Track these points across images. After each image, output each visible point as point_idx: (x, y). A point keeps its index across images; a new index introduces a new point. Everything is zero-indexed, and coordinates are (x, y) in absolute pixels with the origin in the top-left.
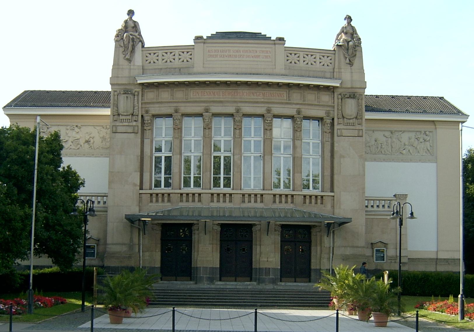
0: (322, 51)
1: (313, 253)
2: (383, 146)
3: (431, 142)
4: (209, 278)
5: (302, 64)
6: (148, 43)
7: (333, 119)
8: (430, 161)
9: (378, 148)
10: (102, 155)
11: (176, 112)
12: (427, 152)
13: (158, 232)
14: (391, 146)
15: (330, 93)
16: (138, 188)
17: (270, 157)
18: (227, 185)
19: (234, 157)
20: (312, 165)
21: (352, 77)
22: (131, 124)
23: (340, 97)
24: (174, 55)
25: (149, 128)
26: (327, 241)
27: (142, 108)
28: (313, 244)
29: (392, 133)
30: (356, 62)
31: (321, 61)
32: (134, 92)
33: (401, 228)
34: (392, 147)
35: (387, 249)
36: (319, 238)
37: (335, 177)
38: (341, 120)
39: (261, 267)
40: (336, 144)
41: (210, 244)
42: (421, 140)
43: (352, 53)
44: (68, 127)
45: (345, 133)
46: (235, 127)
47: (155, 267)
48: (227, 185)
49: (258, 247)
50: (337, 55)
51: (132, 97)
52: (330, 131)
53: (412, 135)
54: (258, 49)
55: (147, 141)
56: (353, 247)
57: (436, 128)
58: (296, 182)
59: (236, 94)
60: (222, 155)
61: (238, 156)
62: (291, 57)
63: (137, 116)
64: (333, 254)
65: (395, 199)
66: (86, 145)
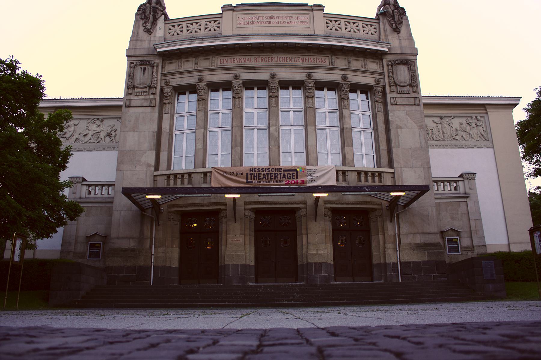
0: (364, 20)
1: (374, 244)
2: (434, 132)
6: (172, 14)
9: (428, 134)
12: (482, 137)
13: (176, 223)
14: (443, 131)
15: (378, 61)
16: (153, 169)
17: (313, 127)
20: (364, 158)
21: (400, 43)
22: (148, 97)
23: (390, 63)
24: (200, 25)
25: (168, 101)
26: (391, 229)
27: (161, 80)
28: (298, 232)
29: (441, 119)
30: (403, 30)
31: (364, 29)
32: (153, 63)
34: (443, 133)
35: (460, 237)
36: (380, 225)
37: (394, 150)
38: (394, 88)
39: (309, 261)
40: (390, 114)
41: (241, 234)
42: (473, 125)
43: (399, 20)
44: (89, 121)
45: (399, 101)
46: (270, 94)
47: (170, 267)
49: (304, 237)
50: (381, 24)
51: (150, 68)
52: (381, 100)
53: (463, 120)
54: (294, 16)
55: (166, 117)
56: (424, 233)
57: (487, 113)
59: (270, 60)
61: (274, 127)
62: (331, 24)
63: (156, 88)
64: (400, 243)
66: (108, 139)
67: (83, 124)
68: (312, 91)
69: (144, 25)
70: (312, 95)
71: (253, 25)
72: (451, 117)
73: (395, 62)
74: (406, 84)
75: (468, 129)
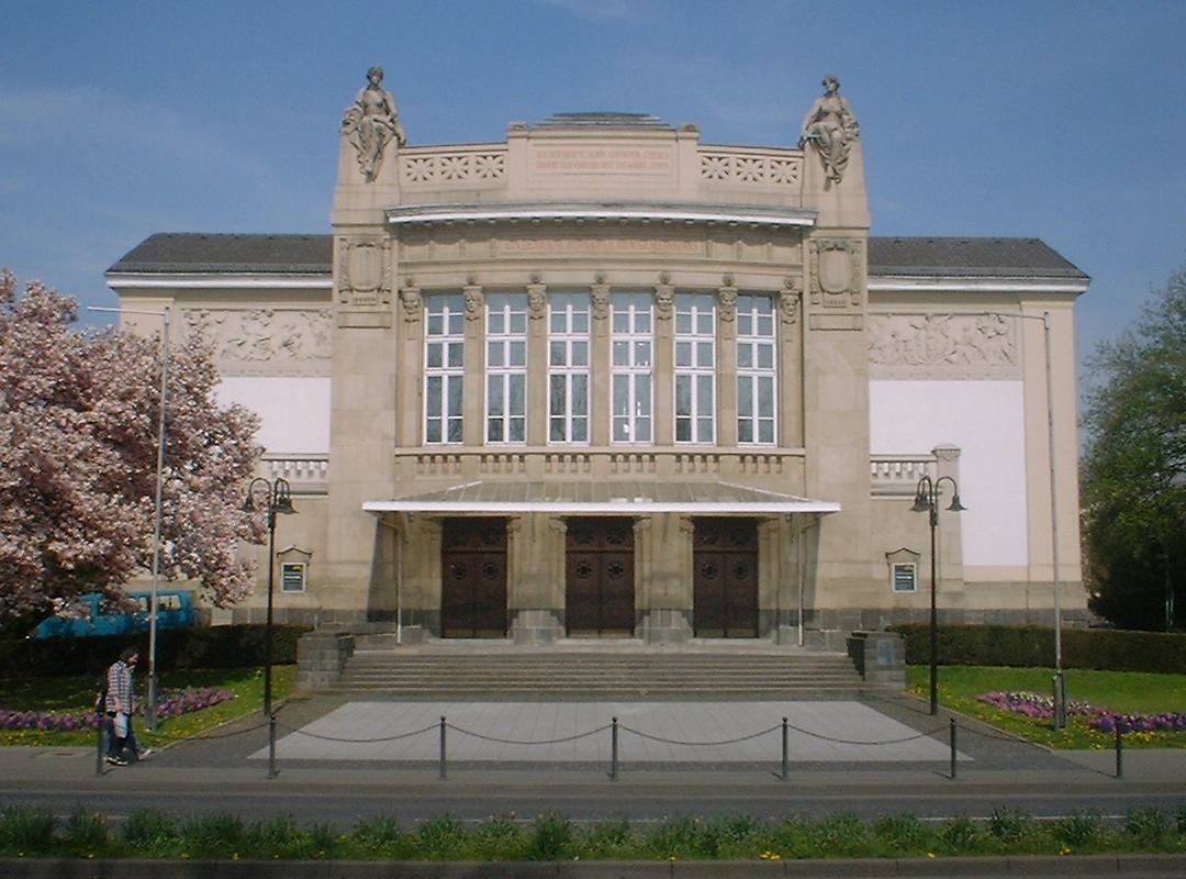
3: (1011, 334)
4: (543, 632)
5: (733, 179)
7: (801, 295)
8: (1008, 376)
10: (318, 373)
11: (471, 284)
14: (927, 346)
16: (393, 444)
18: (579, 435)
19: (592, 378)
22: (376, 309)
29: (927, 319)
33: (933, 530)
44: (246, 314)
45: (826, 322)
46: (596, 313)
48: (579, 435)
56: (845, 561)
58: (724, 427)
60: (569, 370)
65: (934, 458)
67: (234, 320)
68: (669, 307)
69: (360, 159)
70: (667, 314)
71: (567, 171)
72: (946, 315)
73: (824, 246)
74: (841, 290)
75: (979, 339)
